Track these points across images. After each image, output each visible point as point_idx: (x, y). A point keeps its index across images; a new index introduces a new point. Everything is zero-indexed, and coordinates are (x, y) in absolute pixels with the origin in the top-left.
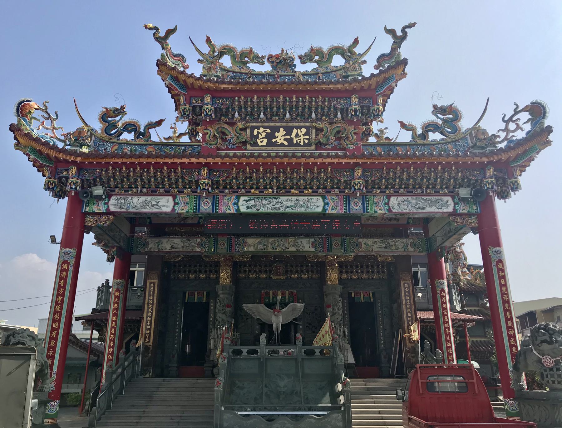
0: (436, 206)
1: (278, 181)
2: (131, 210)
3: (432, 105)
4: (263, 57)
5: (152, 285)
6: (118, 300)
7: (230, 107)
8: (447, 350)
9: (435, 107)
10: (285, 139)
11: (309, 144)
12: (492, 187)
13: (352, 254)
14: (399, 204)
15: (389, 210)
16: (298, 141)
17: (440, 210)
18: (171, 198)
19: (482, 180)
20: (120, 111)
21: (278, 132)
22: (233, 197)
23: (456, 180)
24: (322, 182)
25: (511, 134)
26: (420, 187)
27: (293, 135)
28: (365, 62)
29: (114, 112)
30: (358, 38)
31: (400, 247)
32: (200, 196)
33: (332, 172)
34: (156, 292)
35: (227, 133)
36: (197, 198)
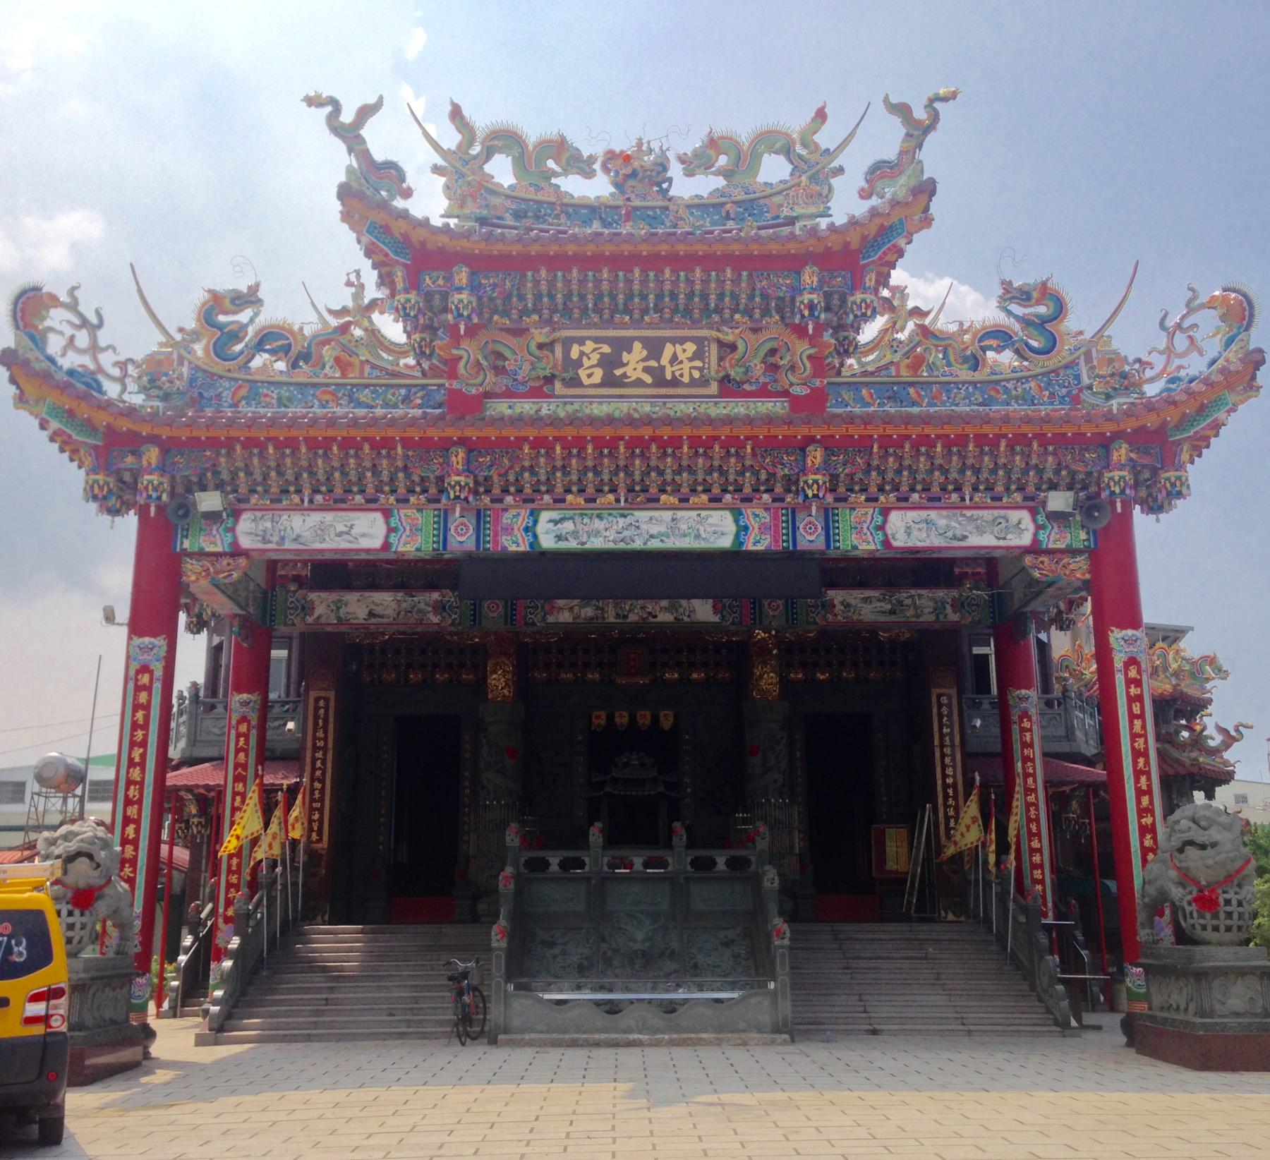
0: (992, 532)
1: (629, 474)
2: (288, 545)
3: (997, 280)
4: (592, 160)
5: (321, 703)
6: (247, 742)
7: (515, 293)
8: (1031, 856)
9: (1007, 285)
10: (646, 370)
11: (704, 382)
12: (1123, 492)
13: (812, 627)
14: (911, 529)
15: (886, 543)
16: (677, 374)
17: (1002, 543)
18: (378, 516)
19: (1101, 474)
20: (249, 299)
21: (629, 352)
22: (525, 513)
23: (1040, 472)
24: (731, 478)
25: (1177, 362)
26: (958, 489)
27: (665, 360)
28: (840, 171)
29: (233, 301)
30: (824, 108)
31: (926, 611)
32: (446, 511)
33: (754, 454)
34: (331, 719)
35: (507, 353)
36: (438, 523)
